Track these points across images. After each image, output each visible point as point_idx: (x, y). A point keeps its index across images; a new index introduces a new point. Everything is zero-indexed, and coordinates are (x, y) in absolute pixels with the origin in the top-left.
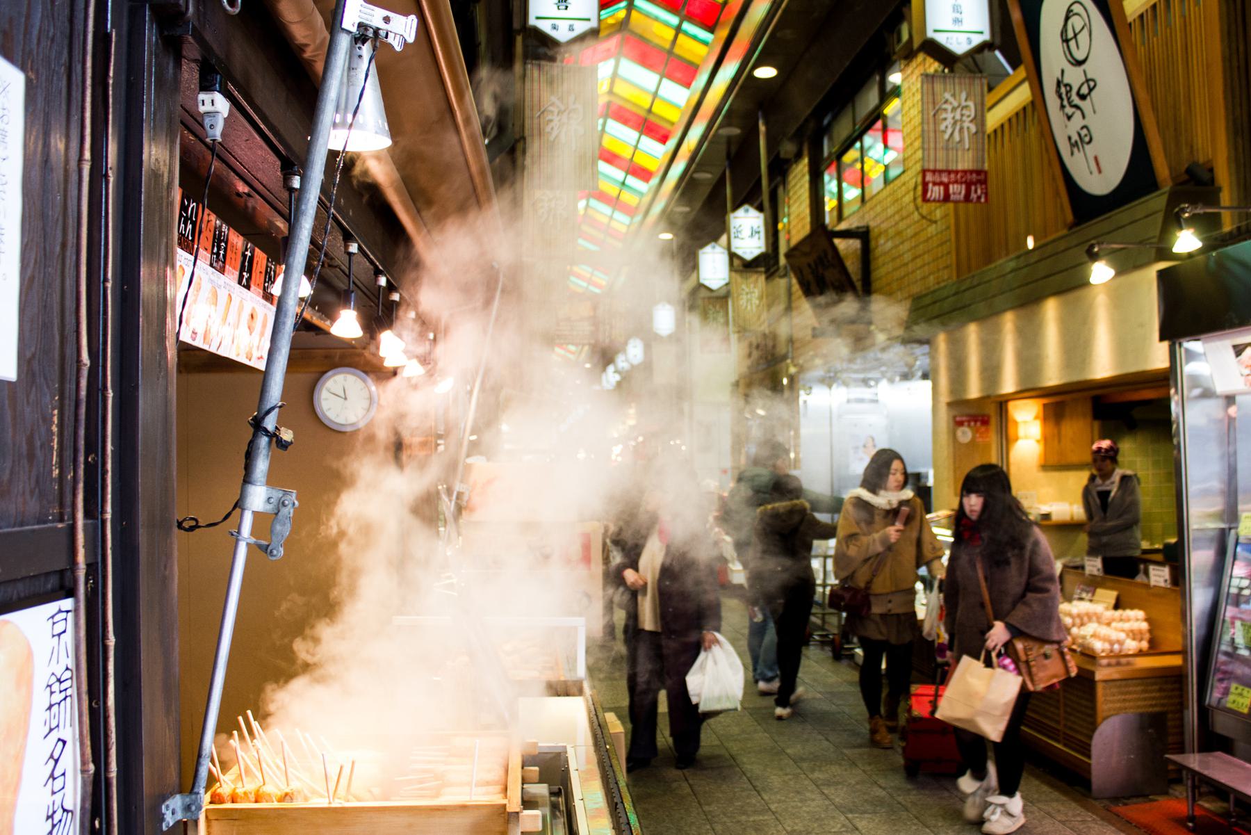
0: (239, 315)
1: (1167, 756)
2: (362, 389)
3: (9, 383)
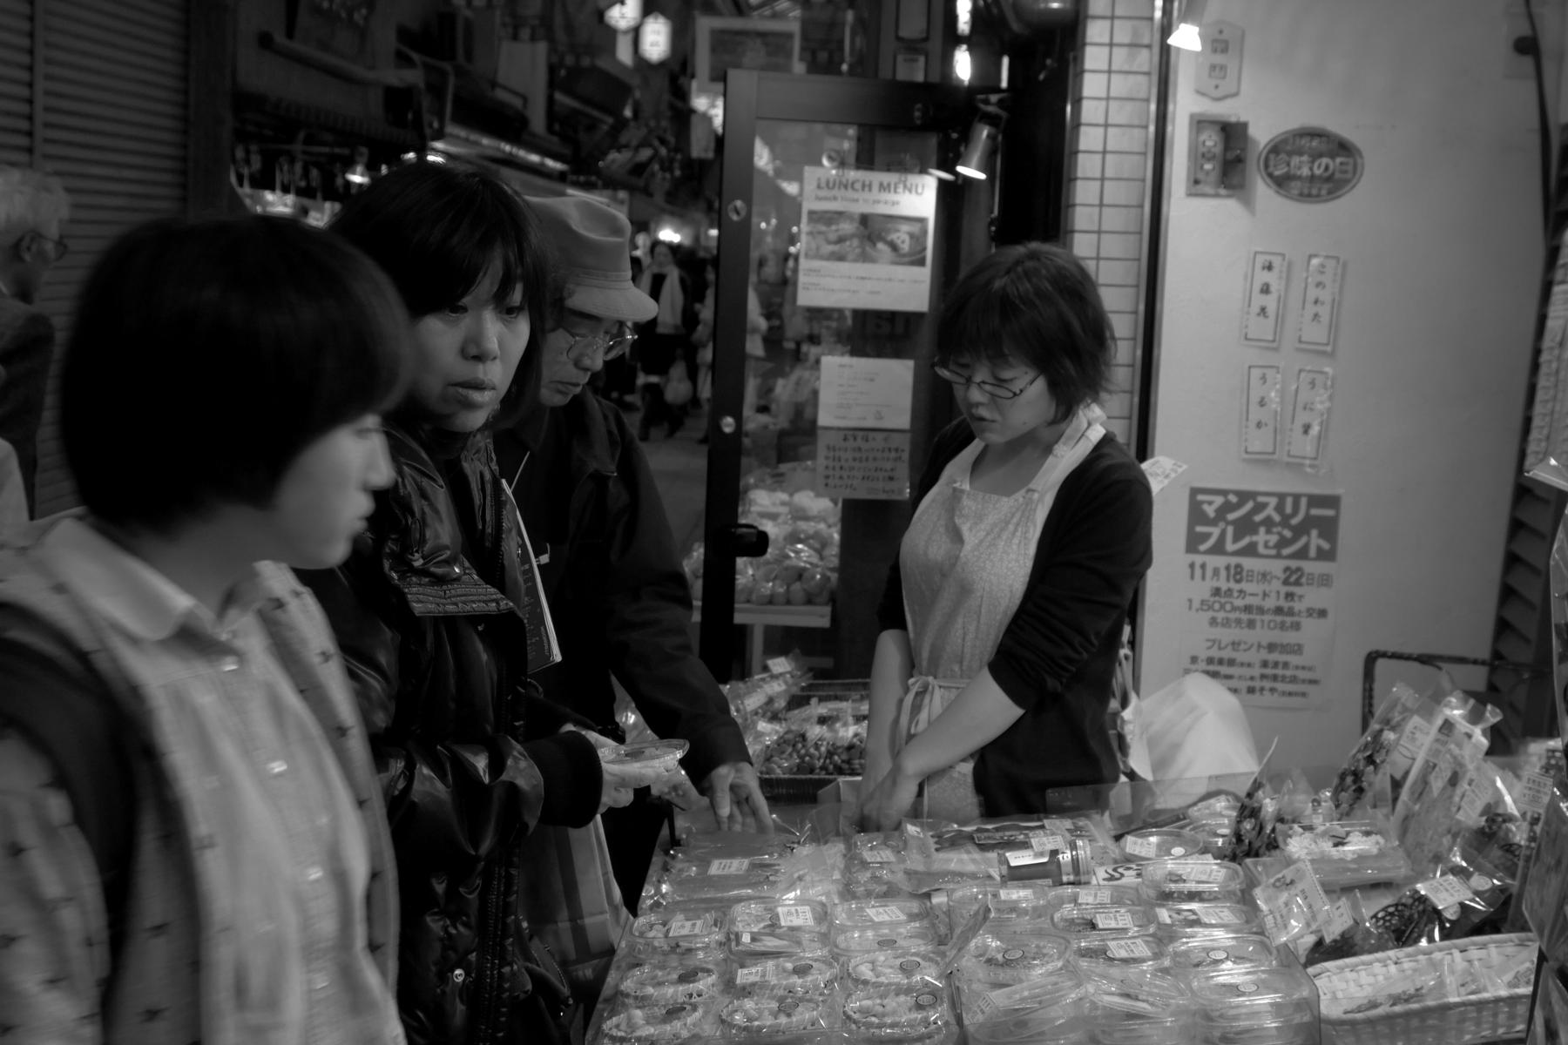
1: (614, 679)
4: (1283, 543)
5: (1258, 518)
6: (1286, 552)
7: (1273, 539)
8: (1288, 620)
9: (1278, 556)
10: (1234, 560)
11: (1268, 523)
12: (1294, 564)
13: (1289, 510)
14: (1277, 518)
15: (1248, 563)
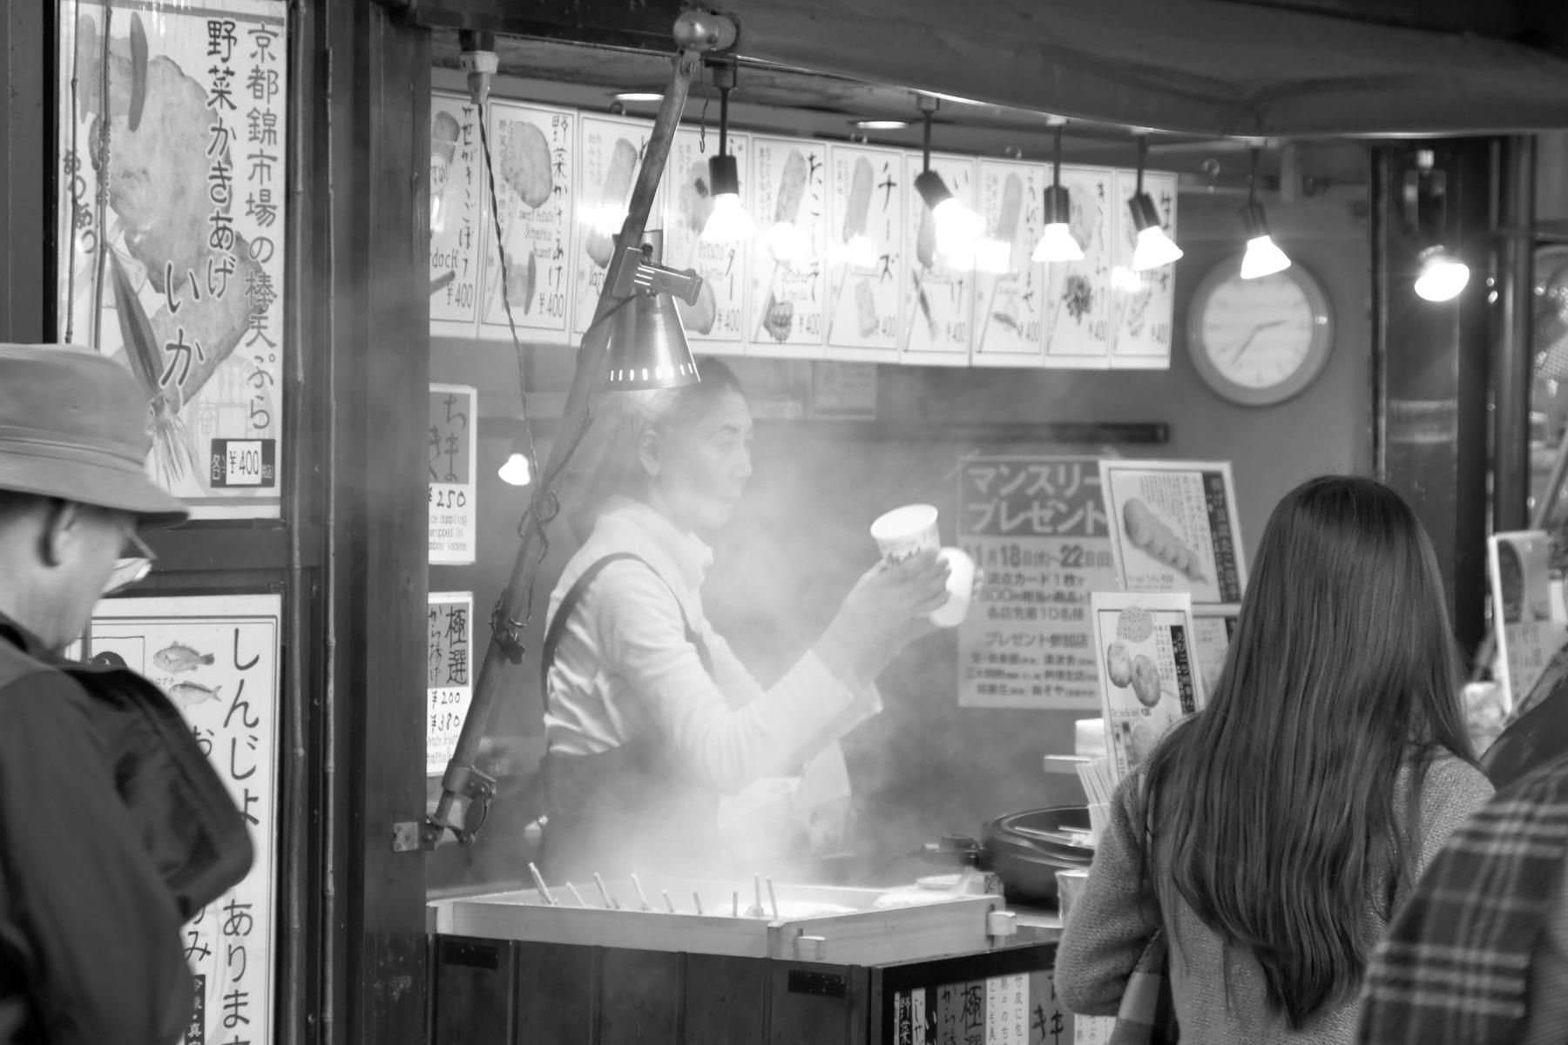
0: (679, 602)
2: (206, 945)
3: (428, 561)
4: (1058, 518)
5: (1031, 491)
6: (1064, 527)
7: (1048, 514)
8: (1070, 607)
9: (1055, 533)
10: (1009, 541)
11: (1042, 497)
12: (1072, 542)
13: (1062, 479)
14: (1050, 489)
15: (1026, 544)
